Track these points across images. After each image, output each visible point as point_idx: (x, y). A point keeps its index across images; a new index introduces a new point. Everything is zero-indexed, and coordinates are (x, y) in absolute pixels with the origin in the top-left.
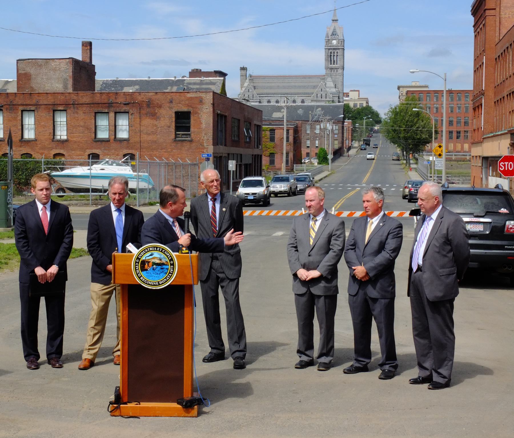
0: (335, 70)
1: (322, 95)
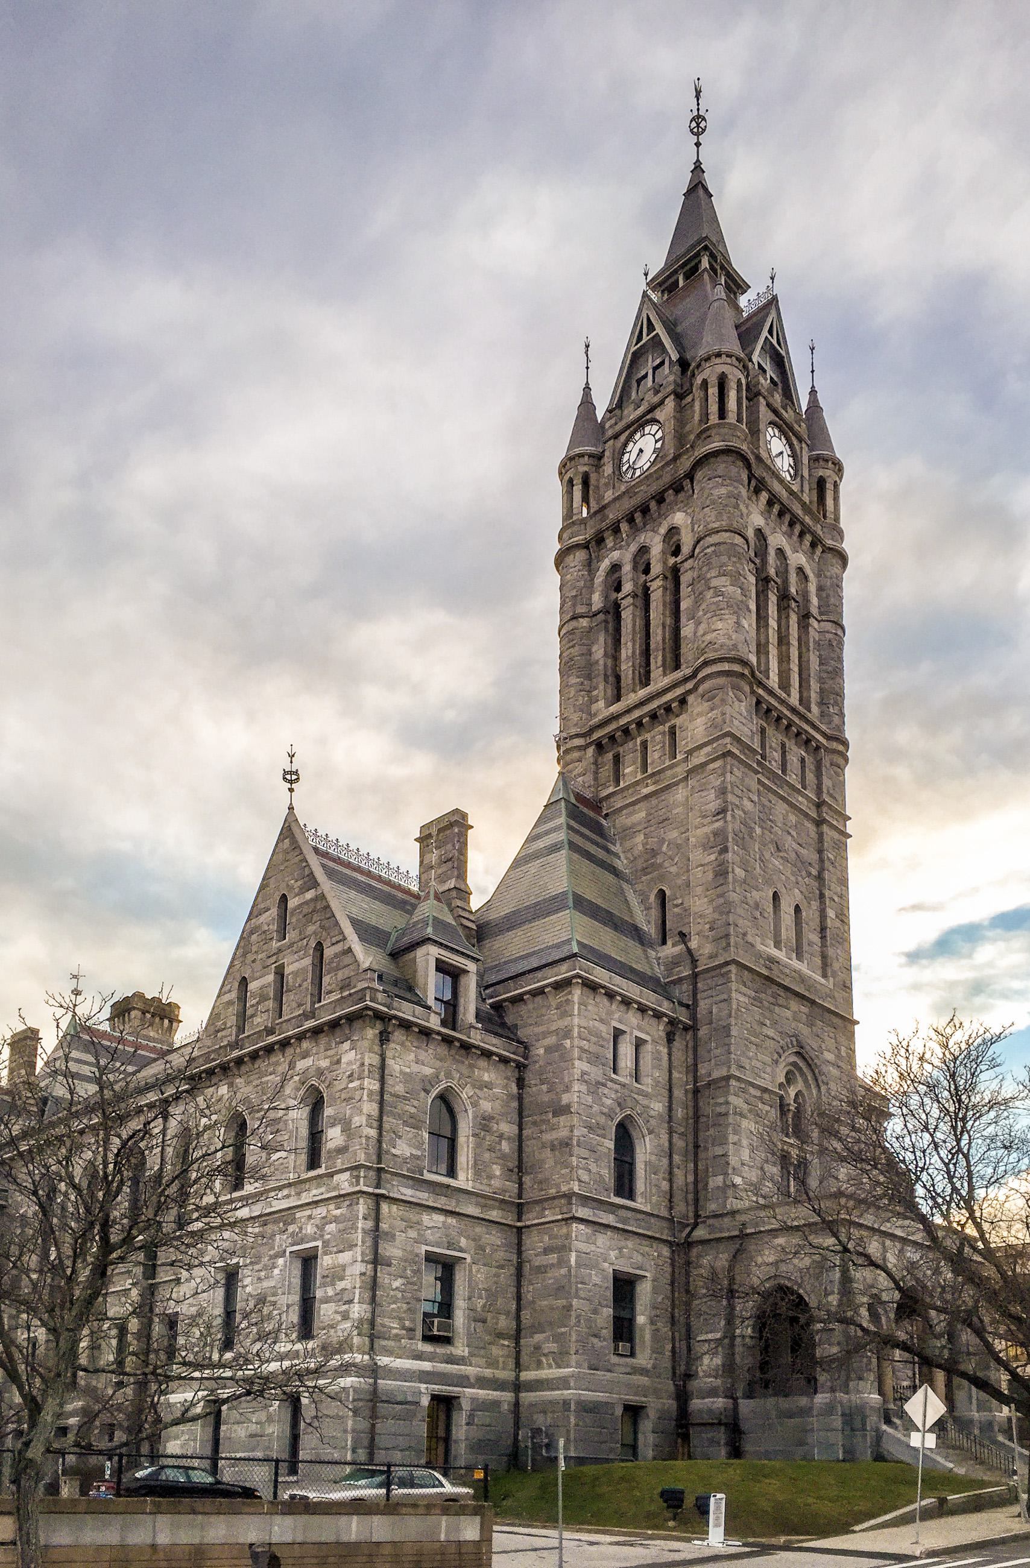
0: (656, 736)
1: (280, 973)
